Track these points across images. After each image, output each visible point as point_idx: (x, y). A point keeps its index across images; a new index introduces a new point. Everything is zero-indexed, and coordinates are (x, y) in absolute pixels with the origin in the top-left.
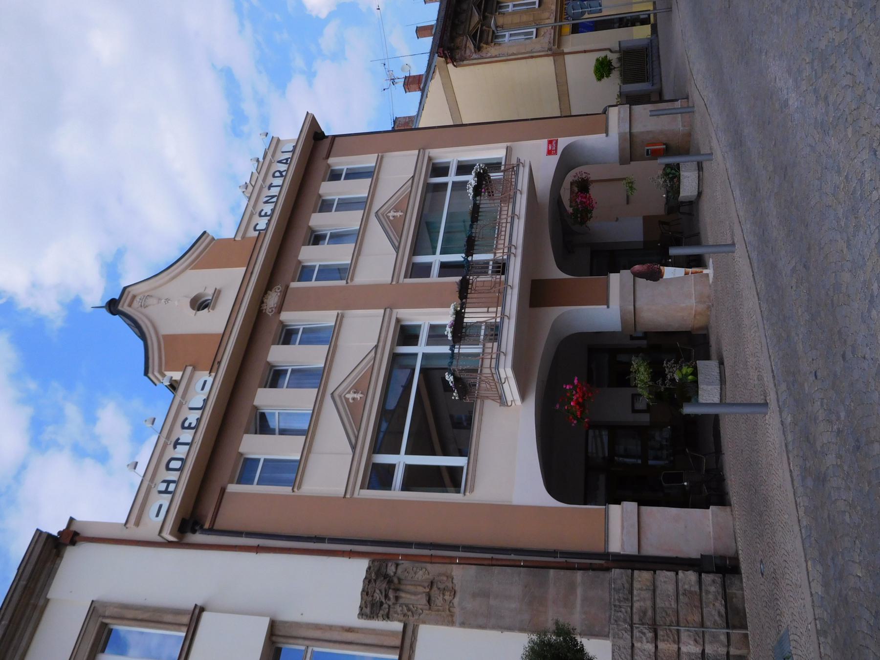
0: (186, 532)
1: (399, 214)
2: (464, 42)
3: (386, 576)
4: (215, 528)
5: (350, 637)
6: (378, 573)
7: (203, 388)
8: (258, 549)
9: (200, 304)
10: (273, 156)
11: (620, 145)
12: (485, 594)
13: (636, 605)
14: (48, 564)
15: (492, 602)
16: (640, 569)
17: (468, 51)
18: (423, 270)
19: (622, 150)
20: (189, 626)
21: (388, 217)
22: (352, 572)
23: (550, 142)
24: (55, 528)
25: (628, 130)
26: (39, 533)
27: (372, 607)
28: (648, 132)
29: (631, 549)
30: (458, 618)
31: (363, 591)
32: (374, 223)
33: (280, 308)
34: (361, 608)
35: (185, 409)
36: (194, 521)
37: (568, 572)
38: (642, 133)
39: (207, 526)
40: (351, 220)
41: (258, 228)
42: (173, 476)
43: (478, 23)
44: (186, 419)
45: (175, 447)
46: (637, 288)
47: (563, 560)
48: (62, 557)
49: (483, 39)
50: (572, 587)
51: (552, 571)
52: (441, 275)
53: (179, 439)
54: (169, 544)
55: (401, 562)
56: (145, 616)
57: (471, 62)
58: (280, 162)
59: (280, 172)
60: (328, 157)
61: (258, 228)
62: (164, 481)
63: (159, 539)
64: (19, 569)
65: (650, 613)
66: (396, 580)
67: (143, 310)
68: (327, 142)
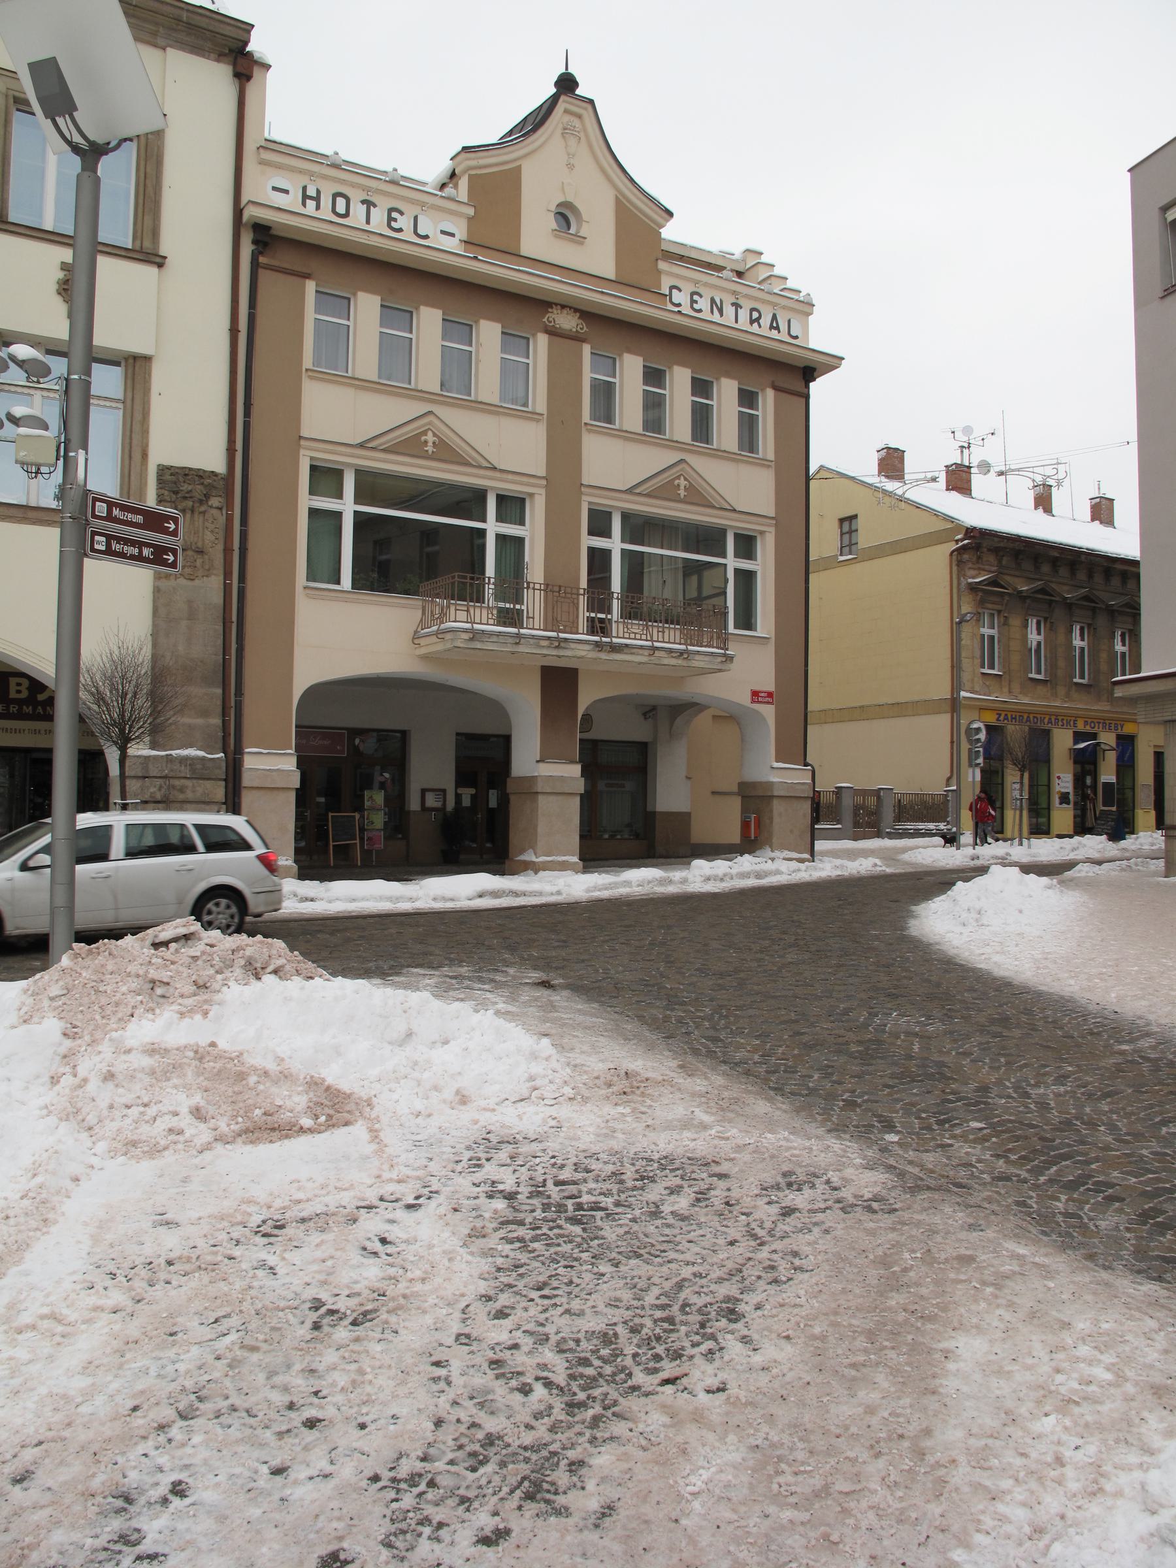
0: (254, 232)
1: (682, 493)
2: (987, 567)
3: (207, 496)
4: (261, 271)
5: (137, 456)
6: (211, 487)
7: (443, 237)
8: (234, 331)
9: (565, 216)
10: (784, 308)
11: (761, 783)
12: (192, 615)
13: (189, 783)
14: (209, 45)
15: (184, 623)
16: (226, 787)
17: (972, 572)
18: (599, 524)
19: (754, 785)
20: (141, 252)
21: (678, 478)
22: (208, 453)
23: (770, 695)
24: (256, 45)
25: (776, 793)
26: (248, 28)
27: (176, 480)
28: (771, 819)
29: (247, 780)
30: (159, 583)
31: (190, 469)
32: (672, 457)
33: (553, 332)
34: (169, 468)
35: (415, 210)
36: (265, 245)
37: (219, 710)
38: (771, 811)
39: (262, 259)
40: (679, 422)
41: (674, 291)
42: (326, 202)
43: (1015, 589)
44: (402, 213)
45: (363, 202)
46: (560, 798)
47: (233, 704)
48: (218, 61)
49: (990, 597)
50: (205, 713)
51: (219, 691)
52: (592, 551)
53: (375, 206)
54: (238, 212)
55: (224, 512)
56: (150, 190)
57: (954, 576)
58: (774, 317)
59: (758, 320)
60: (776, 388)
61: (674, 291)
62: (318, 192)
63: (244, 200)
64: (201, 7)
65: (181, 797)
66: (202, 509)
67: (559, 131)
68: (798, 386)
